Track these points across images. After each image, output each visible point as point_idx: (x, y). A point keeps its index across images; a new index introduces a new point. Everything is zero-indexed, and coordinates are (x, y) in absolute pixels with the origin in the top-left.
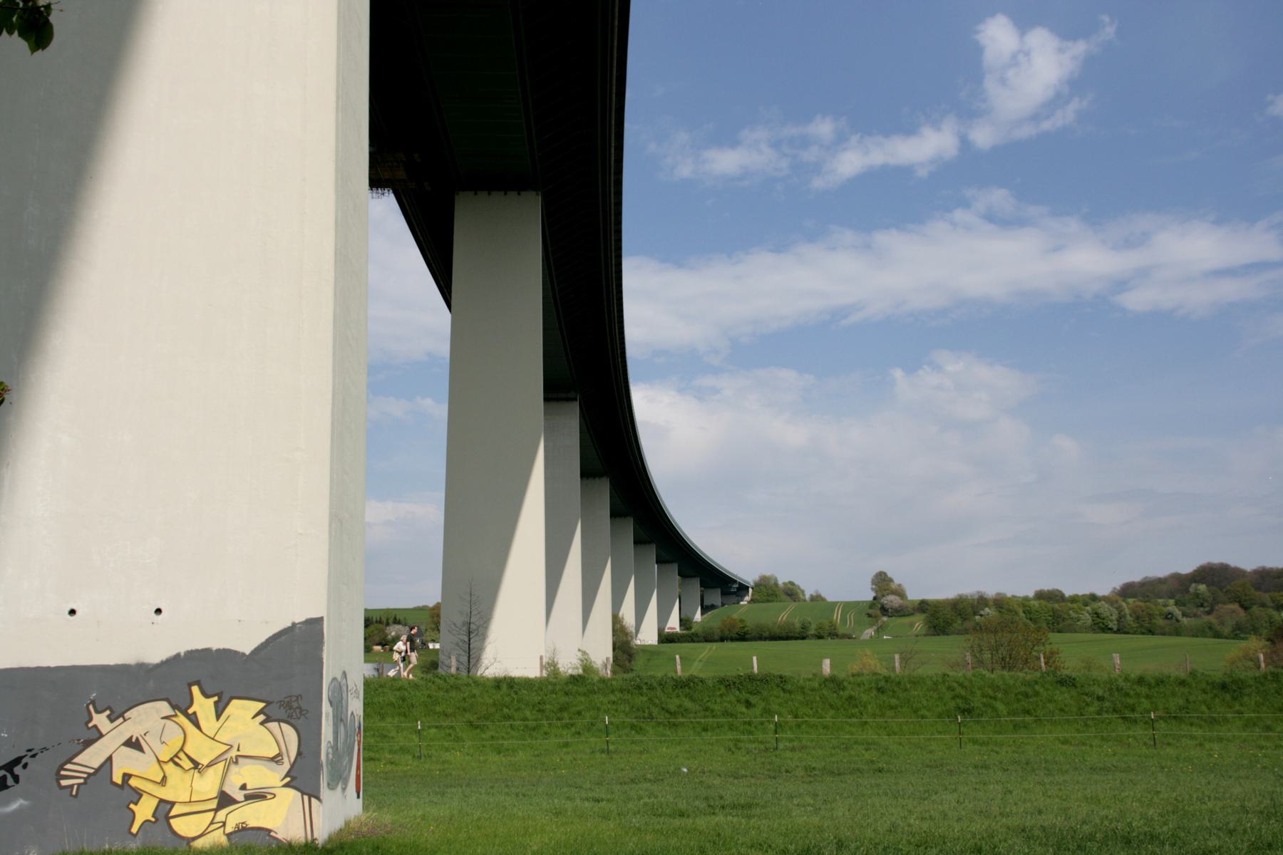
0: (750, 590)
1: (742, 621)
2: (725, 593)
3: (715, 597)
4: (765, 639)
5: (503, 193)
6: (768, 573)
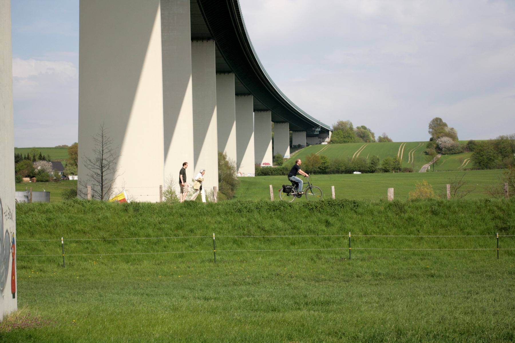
0: (330, 133)
1: (323, 158)
3: (301, 138)
4: (342, 172)
6: (344, 120)
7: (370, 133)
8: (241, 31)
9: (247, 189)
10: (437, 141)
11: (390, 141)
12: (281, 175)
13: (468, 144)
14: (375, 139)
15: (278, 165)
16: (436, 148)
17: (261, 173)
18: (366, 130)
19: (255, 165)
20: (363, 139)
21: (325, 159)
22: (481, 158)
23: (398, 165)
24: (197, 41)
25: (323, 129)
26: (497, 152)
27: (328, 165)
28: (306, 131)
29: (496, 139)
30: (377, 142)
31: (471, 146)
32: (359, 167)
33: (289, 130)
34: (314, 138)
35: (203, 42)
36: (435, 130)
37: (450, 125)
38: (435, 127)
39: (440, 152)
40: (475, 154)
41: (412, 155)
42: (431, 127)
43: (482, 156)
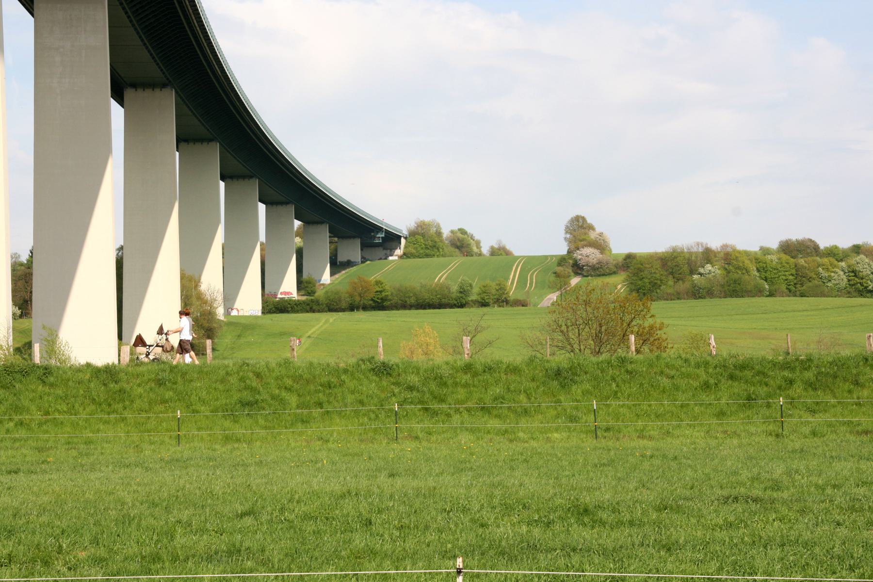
0: (403, 241)
1: (378, 283)
3: (352, 250)
4: (411, 307)
6: (427, 218)
7: (473, 240)
8: (220, 73)
9: (239, 336)
10: (575, 255)
11: (508, 253)
12: (307, 312)
13: (625, 260)
14: (480, 251)
15: (307, 295)
16: (572, 267)
17: (274, 309)
20: (459, 249)
21: (383, 285)
22: (640, 282)
24: (144, 90)
25: (388, 233)
26: (666, 273)
27: (387, 295)
28: (361, 238)
29: (664, 251)
30: (488, 255)
31: (629, 262)
32: (439, 298)
33: (328, 234)
34: (377, 248)
35: (153, 90)
36: (574, 236)
37: (599, 229)
38: (575, 230)
39: (580, 272)
40: (631, 275)
41: (533, 277)
42: (568, 230)
43: (641, 280)
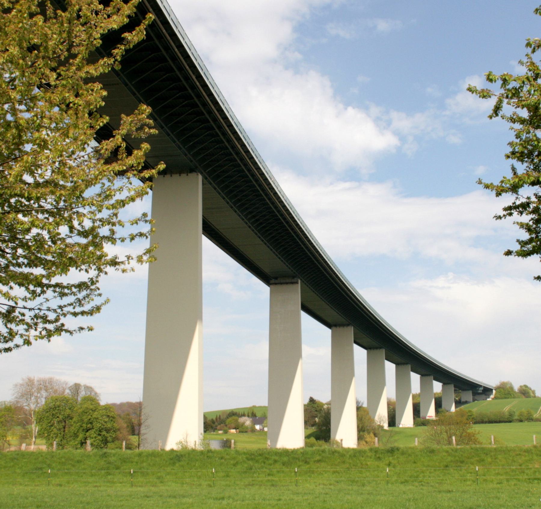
0: (494, 391)
2: (475, 394)
3: (468, 396)
4: (486, 422)
5: (178, 175)
6: (505, 380)
18: (527, 388)
19: (204, 423)
23: (531, 416)
28: (472, 390)
